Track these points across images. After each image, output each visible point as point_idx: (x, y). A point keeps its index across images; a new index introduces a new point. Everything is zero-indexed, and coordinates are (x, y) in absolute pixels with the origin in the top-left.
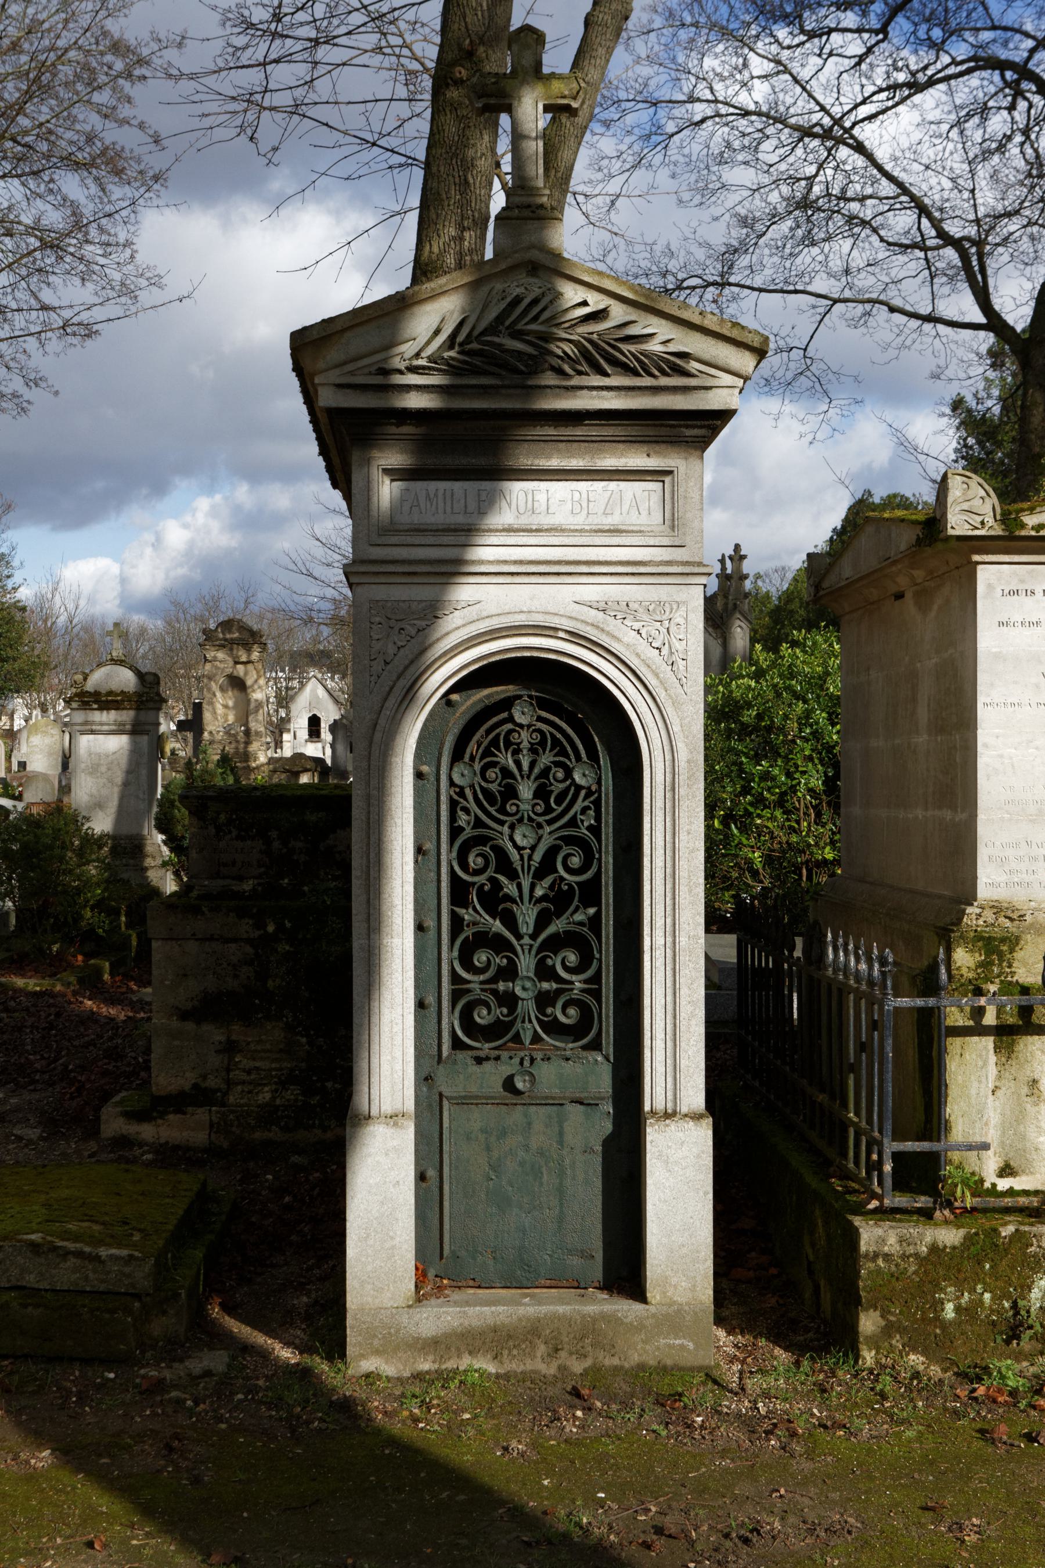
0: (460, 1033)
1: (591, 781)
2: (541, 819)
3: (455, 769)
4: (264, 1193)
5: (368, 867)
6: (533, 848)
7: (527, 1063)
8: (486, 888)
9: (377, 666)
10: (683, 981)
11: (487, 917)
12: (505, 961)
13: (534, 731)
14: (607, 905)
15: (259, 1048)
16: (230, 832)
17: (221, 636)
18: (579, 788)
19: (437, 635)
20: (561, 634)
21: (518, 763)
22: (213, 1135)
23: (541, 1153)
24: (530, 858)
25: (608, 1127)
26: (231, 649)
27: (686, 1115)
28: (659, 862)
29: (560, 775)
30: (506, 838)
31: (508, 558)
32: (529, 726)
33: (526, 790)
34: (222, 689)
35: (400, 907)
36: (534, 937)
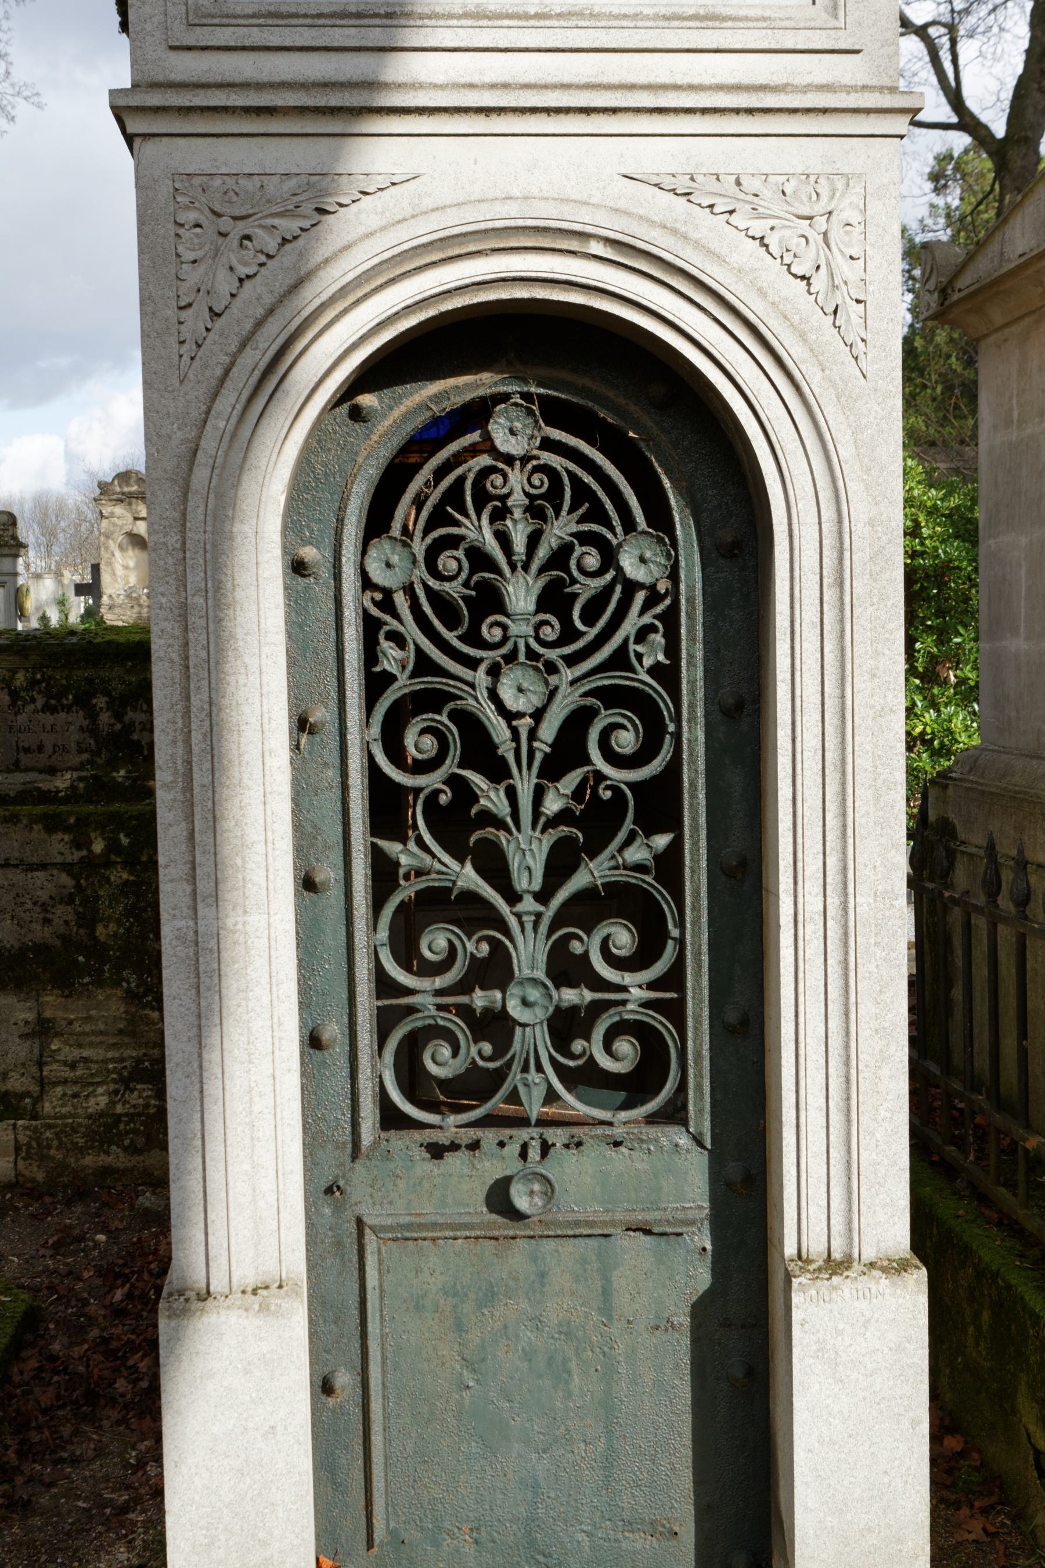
0: (395, 1095)
1: (656, 571)
2: (553, 654)
3: (373, 552)
4: (86, 1275)
5: (189, 763)
6: (538, 715)
7: (534, 1154)
8: (444, 799)
9: (195, 320)
10: (865, 986)
11: (446, 858)
12: (485, 947)
13: (536, 469)
14: (695, 828)
15: (87, 1028)
16: (33, 700)
17: (118, 489)
18: (631, 587)
19: (323, 251)
20: (596, 248)
21: (504, 539)
22: (21, 1164)
23: (567, 1332)
24: (533, 735)
25: (703, 1278)
26: (130, 504)
27: (872, 1265)
28: (809, 739)
29: (592, 561)
30: (483, 695)
31: (476, 79)
32: (525, 459)
33: (521, 594)
34: (121, 548)
35: (260, 848)
36: (543, 896)
